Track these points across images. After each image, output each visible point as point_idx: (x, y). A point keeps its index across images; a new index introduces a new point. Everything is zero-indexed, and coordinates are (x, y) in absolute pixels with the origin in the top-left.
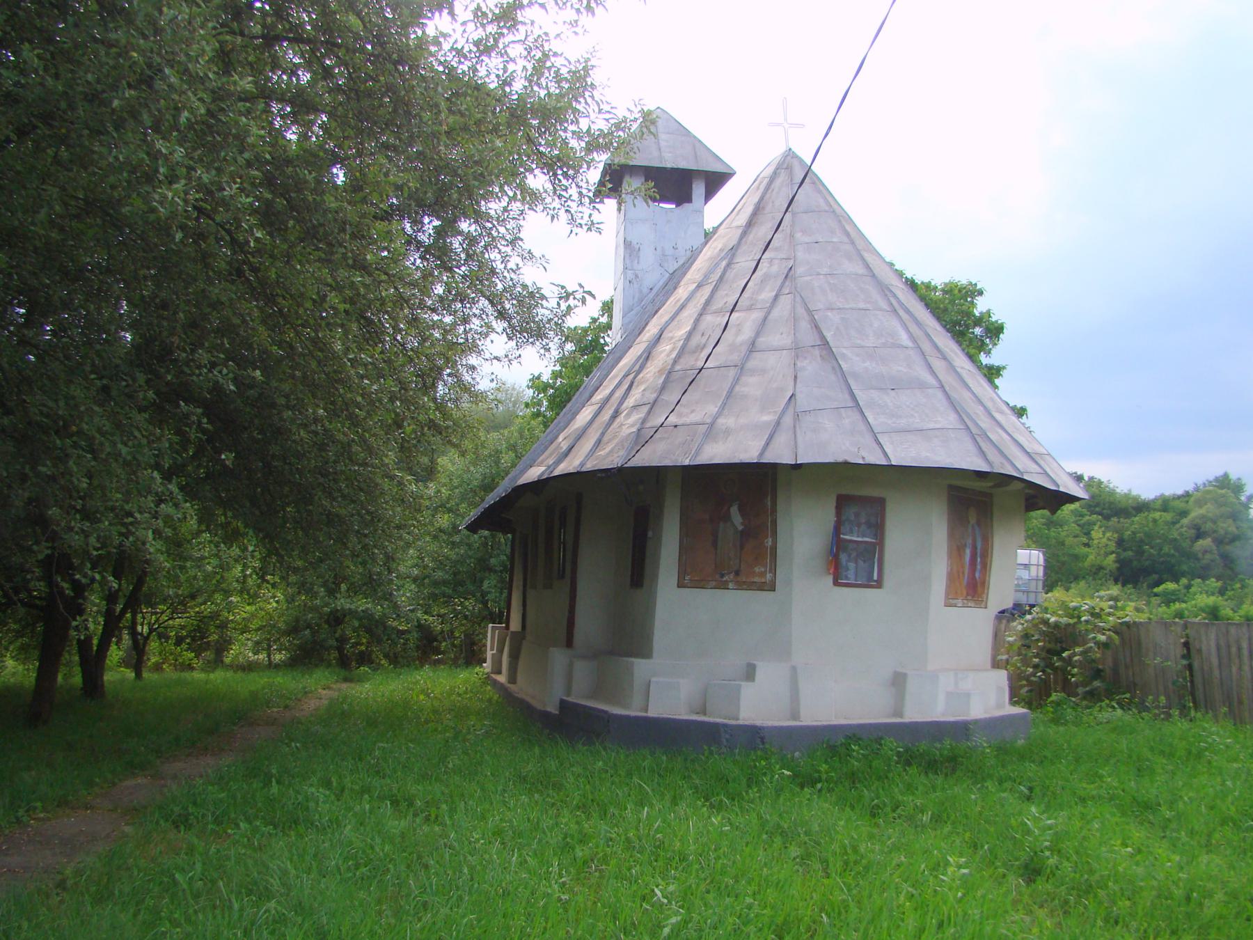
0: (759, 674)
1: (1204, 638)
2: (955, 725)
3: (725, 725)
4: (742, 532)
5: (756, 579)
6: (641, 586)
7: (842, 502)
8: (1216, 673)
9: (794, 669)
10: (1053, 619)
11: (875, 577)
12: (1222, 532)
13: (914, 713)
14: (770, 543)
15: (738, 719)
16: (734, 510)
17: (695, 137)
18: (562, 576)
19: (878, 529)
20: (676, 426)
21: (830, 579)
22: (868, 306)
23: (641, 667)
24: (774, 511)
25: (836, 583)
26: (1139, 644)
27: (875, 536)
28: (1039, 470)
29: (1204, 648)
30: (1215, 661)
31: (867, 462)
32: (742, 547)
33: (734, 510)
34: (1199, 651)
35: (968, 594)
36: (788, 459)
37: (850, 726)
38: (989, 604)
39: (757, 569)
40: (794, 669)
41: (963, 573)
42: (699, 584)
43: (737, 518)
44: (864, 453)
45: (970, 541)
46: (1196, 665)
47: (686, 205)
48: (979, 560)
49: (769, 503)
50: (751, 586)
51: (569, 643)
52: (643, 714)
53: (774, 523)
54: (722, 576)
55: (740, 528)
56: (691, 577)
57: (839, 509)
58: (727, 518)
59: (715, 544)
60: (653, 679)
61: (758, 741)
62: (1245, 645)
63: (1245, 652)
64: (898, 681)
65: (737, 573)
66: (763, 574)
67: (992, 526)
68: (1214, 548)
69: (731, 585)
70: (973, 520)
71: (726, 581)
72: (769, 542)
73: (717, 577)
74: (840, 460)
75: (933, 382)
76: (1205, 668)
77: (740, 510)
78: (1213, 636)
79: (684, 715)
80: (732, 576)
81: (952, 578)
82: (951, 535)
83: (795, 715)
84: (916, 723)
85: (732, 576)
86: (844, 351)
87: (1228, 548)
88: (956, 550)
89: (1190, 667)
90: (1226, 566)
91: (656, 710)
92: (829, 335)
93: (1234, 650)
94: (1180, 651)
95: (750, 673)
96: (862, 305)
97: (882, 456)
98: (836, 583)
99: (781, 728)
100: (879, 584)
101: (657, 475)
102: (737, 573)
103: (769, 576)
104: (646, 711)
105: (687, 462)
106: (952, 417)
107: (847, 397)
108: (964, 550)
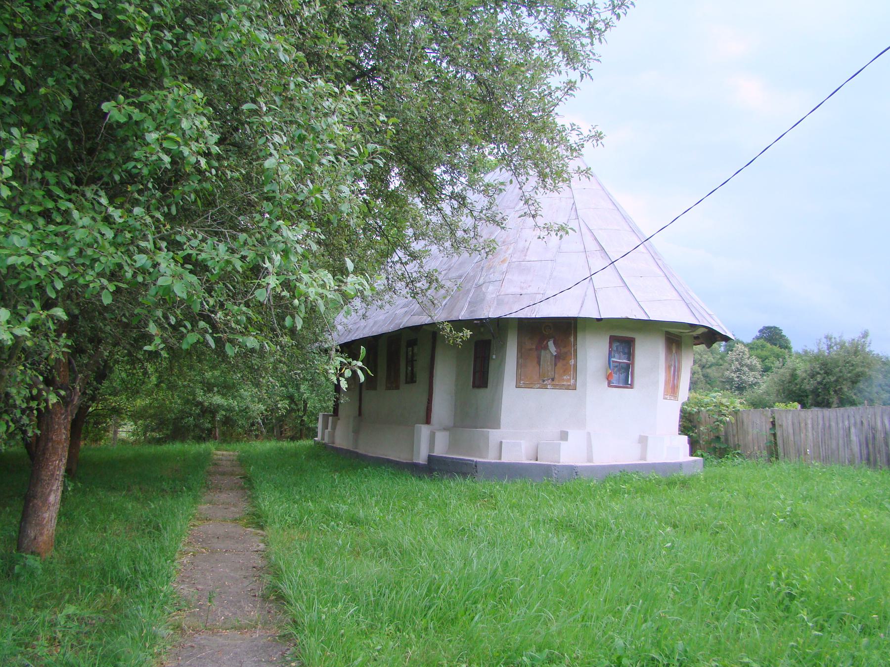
1: (784, 419)
2: (674, 464)
3: (555, 466)
4: (555, 356)
5: (565, 383)
6: (486, 387)
7: (613, 339)
8: (792, 438)
9: (589, 434)
10: (689, 409)
12: (704, 360)
13: (651, 459)
16: (551, 344)
18: (411, 379)
19: (630, 355)
23: (494, 435)
24: (575, 344)
26: (743, 422)
27: (629, 359)
29: (784, 424)
30: (791, 431)
32: (556, 365)
33: (551, 344)
34: (781, 426)
36: (595, 315)
37: (622, 465)
39: (565, 377)
40: (589, 434)
42: (529, 386)
45: (673, 363)
46: (779, 434)
49: (572, 340)
50: (561, 387)
51: (428, 421)
53: (576, 351)
55: (555, 354)
56: (523, 381)
57: (611, 344)
58: (546, 348)
59: (539, 363)
60: (503, 441)
61: (574, 474)
62: (809, 422)
63: (810, 426)
64: (643, 441)
65: (553, 380)
66: (569, 380)
68: (700, 370)
70: (674, 352)
72: (572, 362)
73: (541, 382)
75: (661, 273)
76: (785, 435)
77: (554, 343)
78: (790, 418)
79: (525, 461)
80: (550, 381)
81: (667, 382)
83: (590, 459)
85: (550, 381)
87: (708, 370)
88: (668, 368)
89: (774, 435)
90: (706, 382)
91: (506, 459)
93: (803, 425)
94: (770, 426)
95: (564, 436)
97: (644, 315)
99: (636, 465)
100: (631, 386)
101: (500, 325)
102: (553, 380)
103: (572, 381)
104: (500, 458)
105: (533, 316)
106: (674, 293)
107: (620, 281)
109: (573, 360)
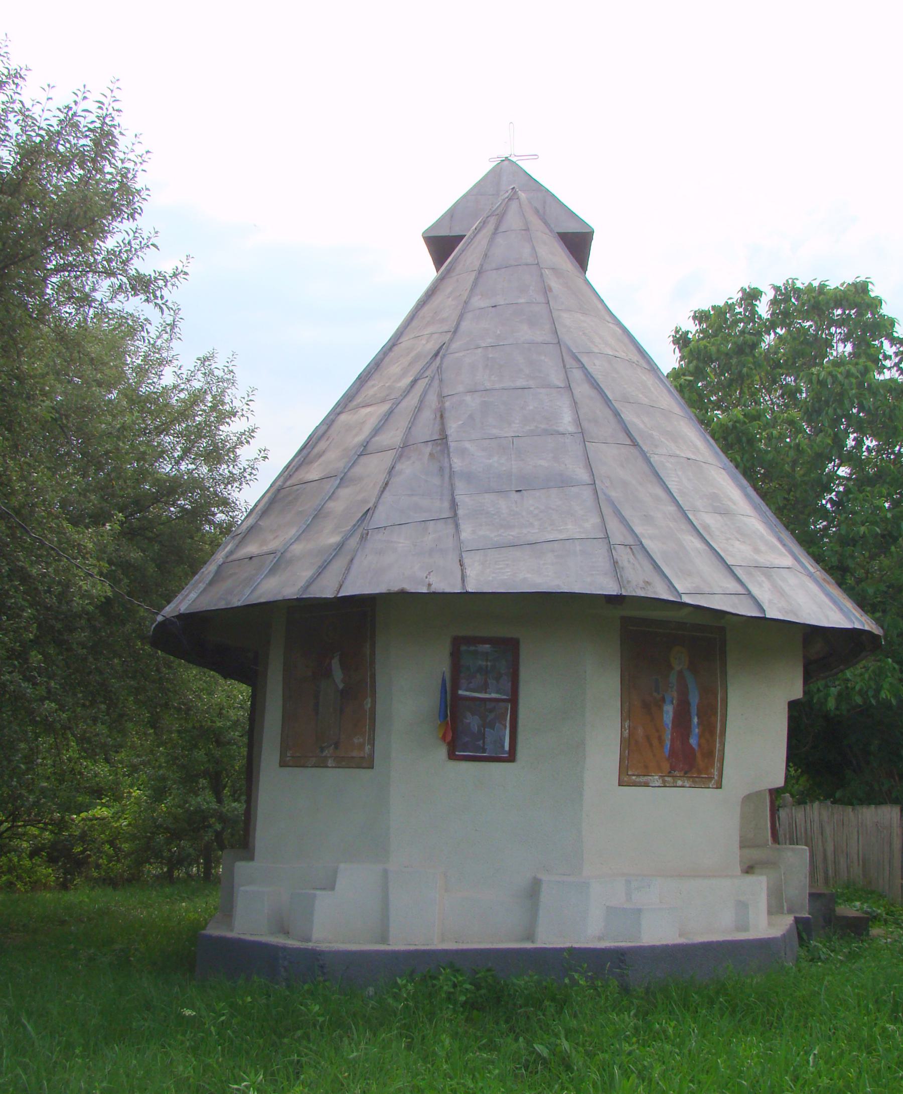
0: (341, 883)
5: (355, 754)
11: (507, 747)
14: (369, 705)
15: (309, 940)
16: (335, 664)
17: (547, 191)
20: (251, 558)
21: (442, 751)
22: (531, 383)
24: (373, 663)
25: (452, 756)
28: (740, 590)
31: (432, 590)
33: (335, 664)
35: (673, 768)
38: (724, 781)
40: (386, 871)
41: (660, 739)
43: (338, 674)
44: (433, 579)
47: (875, 291)
48: (695, 720)
52: (528, 945)
53: (373, 677)
54: (322, 749)
55: (341, 686)
57: (455, 656)
58: (328, 673)
65: (337, 745)
66: (361, 747)
67: (724, 673)
69: (330, 763)
71: (326, 757)
74: (395, 588)
82: (628, 685)
83: (384, 939)
84: (667, 946)
86: (467, 445)
92: (452, 428)
96: (520, 383)
98: (452, 756)
102: (337, 745)
103: (367, 748)
108: (660, 708)
109: (369, 700)
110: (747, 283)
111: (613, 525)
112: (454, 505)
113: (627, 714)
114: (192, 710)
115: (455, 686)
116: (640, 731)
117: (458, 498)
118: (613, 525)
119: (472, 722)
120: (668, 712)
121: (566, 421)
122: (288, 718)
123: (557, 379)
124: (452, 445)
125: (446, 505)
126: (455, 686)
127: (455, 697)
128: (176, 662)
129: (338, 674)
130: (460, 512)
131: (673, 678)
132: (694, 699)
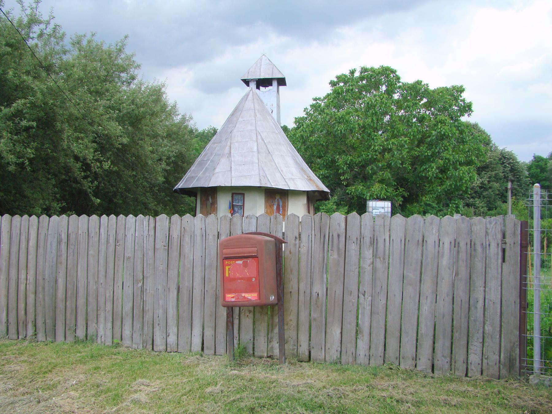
16: (210, 197)
43: (210, 200)
44: (225, 183)
57: (232, 197)
58: (208, 200)
74: (218, 185)
82: (266, 202)
110: (352, 68)
111: (261, 172)
112: (231, 168)
113: (266, 207)
114: (464, 145)
115: (233, 202)
116: (269, 211)
117: (232, 166)
118: (261, 172)
119: (236, 209)
120: (275, 207)
121: (255, 149)
122: (201, 208)
123: (255, 139)
124: (232, 154)
125: (230, 168)
126: (233, 202)
127: (233, 205)
128: (184, 196)
129: (210, 200)
130: (232, 169)
131: (276, 200)
132: (281, 204)
